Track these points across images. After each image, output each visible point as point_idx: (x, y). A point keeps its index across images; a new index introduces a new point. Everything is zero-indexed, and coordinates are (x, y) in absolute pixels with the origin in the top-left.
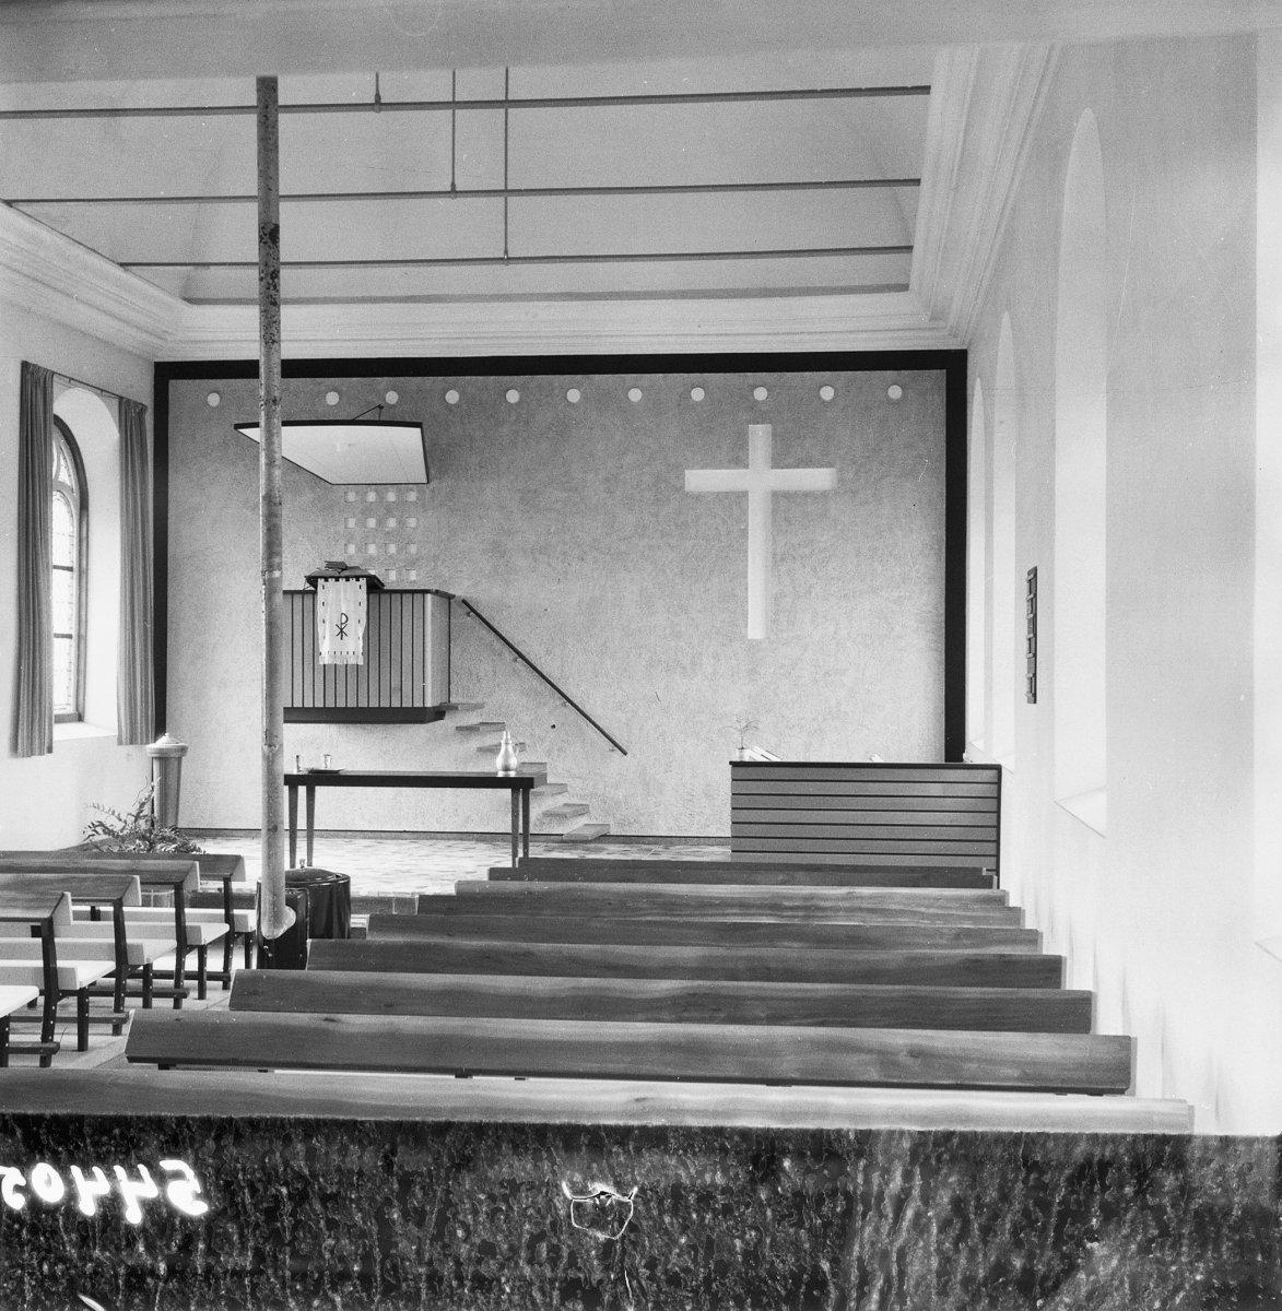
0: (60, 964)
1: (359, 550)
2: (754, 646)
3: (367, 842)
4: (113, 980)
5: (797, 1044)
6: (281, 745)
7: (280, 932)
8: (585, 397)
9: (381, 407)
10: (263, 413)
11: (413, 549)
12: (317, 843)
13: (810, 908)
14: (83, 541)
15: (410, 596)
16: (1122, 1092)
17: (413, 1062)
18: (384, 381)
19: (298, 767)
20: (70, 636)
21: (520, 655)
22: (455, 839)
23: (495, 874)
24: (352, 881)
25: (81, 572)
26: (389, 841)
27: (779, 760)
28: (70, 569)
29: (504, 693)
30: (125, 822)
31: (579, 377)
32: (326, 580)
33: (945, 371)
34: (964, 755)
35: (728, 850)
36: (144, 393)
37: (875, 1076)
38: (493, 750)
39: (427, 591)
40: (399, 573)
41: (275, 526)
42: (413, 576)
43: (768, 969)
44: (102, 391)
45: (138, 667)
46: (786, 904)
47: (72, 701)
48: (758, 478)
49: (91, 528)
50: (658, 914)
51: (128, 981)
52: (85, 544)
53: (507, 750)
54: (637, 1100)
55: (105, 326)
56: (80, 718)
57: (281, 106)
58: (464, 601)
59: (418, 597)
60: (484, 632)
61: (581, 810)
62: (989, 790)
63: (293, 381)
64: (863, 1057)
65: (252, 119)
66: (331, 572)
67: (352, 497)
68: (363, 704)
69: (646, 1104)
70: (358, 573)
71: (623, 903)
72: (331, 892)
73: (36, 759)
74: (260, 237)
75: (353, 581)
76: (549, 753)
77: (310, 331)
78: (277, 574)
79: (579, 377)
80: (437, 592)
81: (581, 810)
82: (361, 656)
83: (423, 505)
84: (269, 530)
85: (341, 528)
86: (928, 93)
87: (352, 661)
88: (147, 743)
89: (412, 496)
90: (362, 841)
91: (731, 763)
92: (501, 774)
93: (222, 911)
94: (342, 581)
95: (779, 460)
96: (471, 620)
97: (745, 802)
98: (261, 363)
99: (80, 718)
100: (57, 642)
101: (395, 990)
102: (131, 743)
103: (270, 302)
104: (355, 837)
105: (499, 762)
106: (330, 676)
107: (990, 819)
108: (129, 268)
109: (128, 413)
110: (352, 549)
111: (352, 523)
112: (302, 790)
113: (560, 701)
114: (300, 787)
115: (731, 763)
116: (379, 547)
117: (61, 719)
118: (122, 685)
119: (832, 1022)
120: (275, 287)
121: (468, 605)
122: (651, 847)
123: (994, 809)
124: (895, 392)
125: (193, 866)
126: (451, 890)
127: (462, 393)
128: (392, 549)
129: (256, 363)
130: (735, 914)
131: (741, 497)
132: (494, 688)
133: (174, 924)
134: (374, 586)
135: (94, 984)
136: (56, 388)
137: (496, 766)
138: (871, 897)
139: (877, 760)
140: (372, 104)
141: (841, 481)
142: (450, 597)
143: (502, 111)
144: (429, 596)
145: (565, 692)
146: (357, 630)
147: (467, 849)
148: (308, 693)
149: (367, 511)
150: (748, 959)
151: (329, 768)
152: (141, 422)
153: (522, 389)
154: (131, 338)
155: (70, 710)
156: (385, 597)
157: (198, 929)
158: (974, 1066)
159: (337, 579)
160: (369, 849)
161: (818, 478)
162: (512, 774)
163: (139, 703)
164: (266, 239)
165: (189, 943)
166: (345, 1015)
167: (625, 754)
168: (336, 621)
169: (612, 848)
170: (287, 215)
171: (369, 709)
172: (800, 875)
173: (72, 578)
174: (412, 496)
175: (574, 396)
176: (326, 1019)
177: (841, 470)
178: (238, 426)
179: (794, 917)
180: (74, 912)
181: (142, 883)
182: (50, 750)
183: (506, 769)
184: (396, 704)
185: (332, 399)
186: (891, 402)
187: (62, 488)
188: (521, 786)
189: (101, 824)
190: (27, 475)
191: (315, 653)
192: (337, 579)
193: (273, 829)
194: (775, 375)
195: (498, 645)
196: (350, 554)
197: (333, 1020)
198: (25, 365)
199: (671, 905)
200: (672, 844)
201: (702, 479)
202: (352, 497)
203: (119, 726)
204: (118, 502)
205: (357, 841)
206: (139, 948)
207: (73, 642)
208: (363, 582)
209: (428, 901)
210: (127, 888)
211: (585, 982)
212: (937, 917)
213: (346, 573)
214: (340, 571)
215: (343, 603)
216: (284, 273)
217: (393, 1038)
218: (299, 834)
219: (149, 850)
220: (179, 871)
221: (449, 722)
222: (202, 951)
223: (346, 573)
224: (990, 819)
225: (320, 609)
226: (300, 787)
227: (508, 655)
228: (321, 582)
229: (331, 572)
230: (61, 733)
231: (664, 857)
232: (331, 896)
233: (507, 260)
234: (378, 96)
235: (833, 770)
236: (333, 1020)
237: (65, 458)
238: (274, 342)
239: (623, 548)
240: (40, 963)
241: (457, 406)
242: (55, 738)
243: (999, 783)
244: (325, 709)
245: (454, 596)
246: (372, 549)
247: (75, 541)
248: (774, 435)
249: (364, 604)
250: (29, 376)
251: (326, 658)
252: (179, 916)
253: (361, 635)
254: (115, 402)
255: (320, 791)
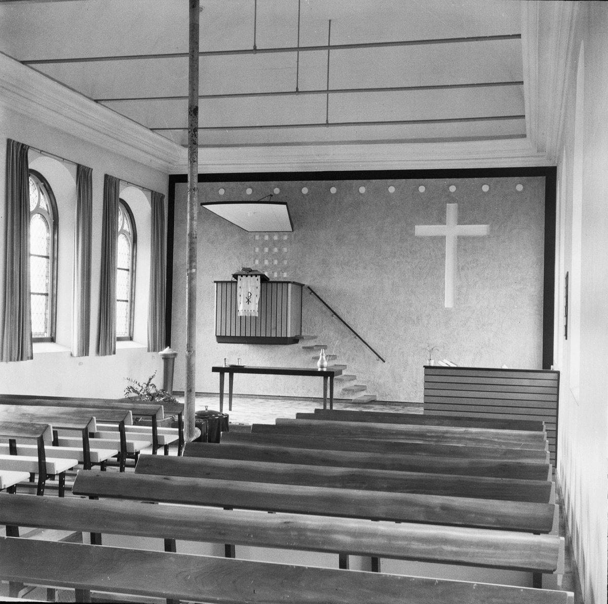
0: (91, 450)
1: (260, 263)
2: (448, 312)
3: (262, 400)
4: (116, 459)
5: (386, 501)
6: (194, 352)
7: (193, 439)
8: (367, 191)
9: (271, 195)
10: (189, 195)
11: (285, 262)
12: (234, 401)
13: (442, 437)
14: (134, 257)
15: (286, 284)
16: (547, 533)
17: (205, 501)
18: (273, 183)
19: (225, 364)
20: (127, 301)
21: (335, 313)
22: (302, 400)
23: (299, 416)
24: (230, 417)
25: (133, 271)
26: (272, 401)
27: (455, 366)
28: (128, 270)
29: (328, 331)
30: (142, 387)
31: (365, 181)
32: (242, 276)
33: (545, 177)
34: (552, 366)
35: (422, 409)
36: (164, 189)
37: (422, 518)
38: (317, 358)
39: (289, 282)
40: (279, 273)
41: (193, 248)
42: (285, 275)
43: (401, 465)
44: (143, 188)
45: (158, 317)
46: (428, 434)
47: (128, 331)
48: (451, 230)
49: (138, 250)
50: (365, 437)
51: (127, 459)
52: (135, 259)
53: (322, 359)
54: (285, 523)
55: (145, 159)
56: (131, 339)
57: (200, 53)
58: (309, 287)
59: (285, 285)
60: (317, 302)
61: (363, 389)
62: (554, 383)
63: (201, 183)
64: (417, 509)
65: (186, 60)
66: (244, 272)
67: (257, 237)
68: (258, 335)
69: (290, 525)
70: (256, 273)
71: (351, 432)
72: (219, 422)
73: (108, 357)
74: (189, 113)
75: (254, 277)
76: (348, 360)
77: (212, 161)
78: (194, 270)
79: (365, 181)
80: (294, 283)
81: (363, 389)
82: (257, 312)
83: (291, 242)
84: (190, 250)
85: (252, 252)
86: (520, 38)
87: (253, 315)
88: (159, 351)
89: (286, 238)
90: (259, 400)
91: (424, 367)
92: (319, 370)
93: (177, 430)
94: (249, 277)
95: (461, 221)
96: (312, 296)
97: (431, 385)
98: (189, 175)
99: (131, 339)
100: (118, 304)
101: (214, 467)
102: (154, 351)
103: (193, 145)
104: (256, 398)
105: (319, 363)
106: (243, 321)
107: (553, 398)
108: (155, 131)
109: (156, 199)
110: (257, 262)
111: (257, 250)
112: (227, 375)
113: (353, 336)
114: (225, 373)
115: (424, 367)
116: (269, 261)
117: (119, 339)
118: (150, 324)
119: (455, 494)
120: (195, 136)
121: (311, 290)
122: (395, 407)
123: (556, 393)
124: (520, 188)
125: (161, 407)
126: (273, 423)
127: (310, 189)
128: (276, 262)
129: (186, 176)
130: (403, 439)
131: (442, 239)
132: (321, 328)
133: (152, 434)
134: (264, 280)
135: (106, 460)
136: (121, 186)
137: (317, 366)
138: (476, 433)
139: (505, 367)
140: (252, 50)
141: (491, 230)
142: (302, 285)
143: (296, 52)
144: (290, 285)
145: (356, 331)
146: (255, 300)
147: (306, 405)
148: (233, 329)
149: (265, 244)
150: (393, 459)
151: (240, 365)
152: (162, 203)
153: (338, 187)
154: (158, 163)
155: (127, 335)
156: (269, 285)
157: (163, 437)
158: (473, 515)
159: (252, 276)
160: (261, 404)
161: (480, 230)
162: (325, 370)
163: (158, 330)
164: (192, 113)
165: (159, 443)
166: (173, 477)
167: (384, 362)
168: (246, 296)
169: (377, 407)
170: (202, 104)
171: (276, 338)
172: (446, 421)
173: (128, 274)
174: (286, 238)
175: (362, 190)
176: (165, 478)
177: (492, 226)
178: (202, 204)
179: (431, 441)
180: (97, 426)
181: (133, 415)
182: (114, 353)
183: (322, 367)
184: (273, 335)
185: (249, 191)
186: (517, 192)
187: (123, 232)
188: (329, 375)
189: (132, 387)
190: (106, 226)
191: (236, 310)
192: (247, 276)
193: (221, 395)
194: (460, 179)
195: (325, 308)
196: (255, 264)
197: (168, 479)
198: (106, 176)
199: (371, 432)
200: (406, 406)
201: (422, 230)
202: (257, 237)
203: (149, 345)
204: (150, 240)
205: (256, 400)
206: (132, 444)
207: (129, 304)
208: (259, 277)
209: (256, 427)
210: (126, 416)
211: (302, 467)
212: (504, 444)
213: (251, 273)
214: (248, 272)
215: (249, 287)
216: (200, 132)
217: (194, 489)
218: (327, 400)
219: (151, 401)
220: (154, 410)
221: (300, 345)
222: (166, 448)
223: (251, 273)
224: (553, 398)
225: (239, 290)
226: (225, 373)
227: (329, 313)
228: (239, 277)
229: (244, 272)
230: (119, 345)
231: (401, 412)
232: (219, 424)
233: (327, 124)
234: (255, 46)
235: (537, 373)
236: (168, 479)
237: (126, 219)
238: (194, 161)
239: (385, 263)
240: (82, 449)
241: (307, 195)
242: (116, 348)
243: (558, 380)
244: (240, 337)
245: (304, 285)
246: (266, 262)
247: (130, 257)
248: (459, 208)
249: (259, 287)
250: (108, 181)
251: (241, 313)
252: (154, 431)
253: (257, 302)
254: (150, 193)
255: (235, 375)
